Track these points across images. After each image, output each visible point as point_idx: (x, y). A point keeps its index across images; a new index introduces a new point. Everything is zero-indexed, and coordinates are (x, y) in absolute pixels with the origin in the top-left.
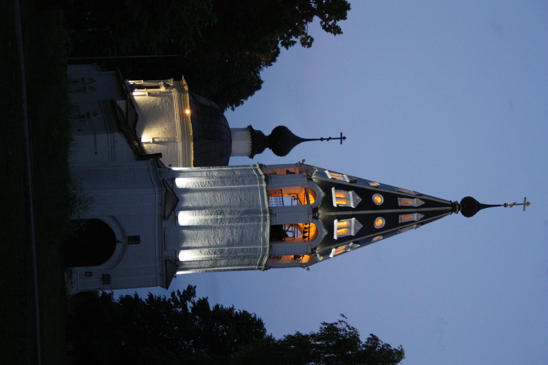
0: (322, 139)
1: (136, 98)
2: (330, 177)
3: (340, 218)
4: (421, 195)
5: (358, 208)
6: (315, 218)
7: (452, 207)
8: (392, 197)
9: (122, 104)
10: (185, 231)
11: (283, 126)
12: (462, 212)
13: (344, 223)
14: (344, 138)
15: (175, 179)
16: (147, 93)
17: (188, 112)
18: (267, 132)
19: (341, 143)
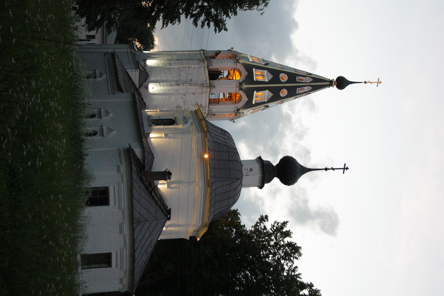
0: (326, 169)
1: (152, 140)
2: (251, 60)
3: (259, 90)
4: (311, 74)
5: (270, 82)
7: (330, 83)
8: (293, 76)
9: (138, 151)
10: (152, 96)
11: (343, 89)
12: (337, 86)
15: (146, 60)
17: (206, 156)
18: (275, 162)
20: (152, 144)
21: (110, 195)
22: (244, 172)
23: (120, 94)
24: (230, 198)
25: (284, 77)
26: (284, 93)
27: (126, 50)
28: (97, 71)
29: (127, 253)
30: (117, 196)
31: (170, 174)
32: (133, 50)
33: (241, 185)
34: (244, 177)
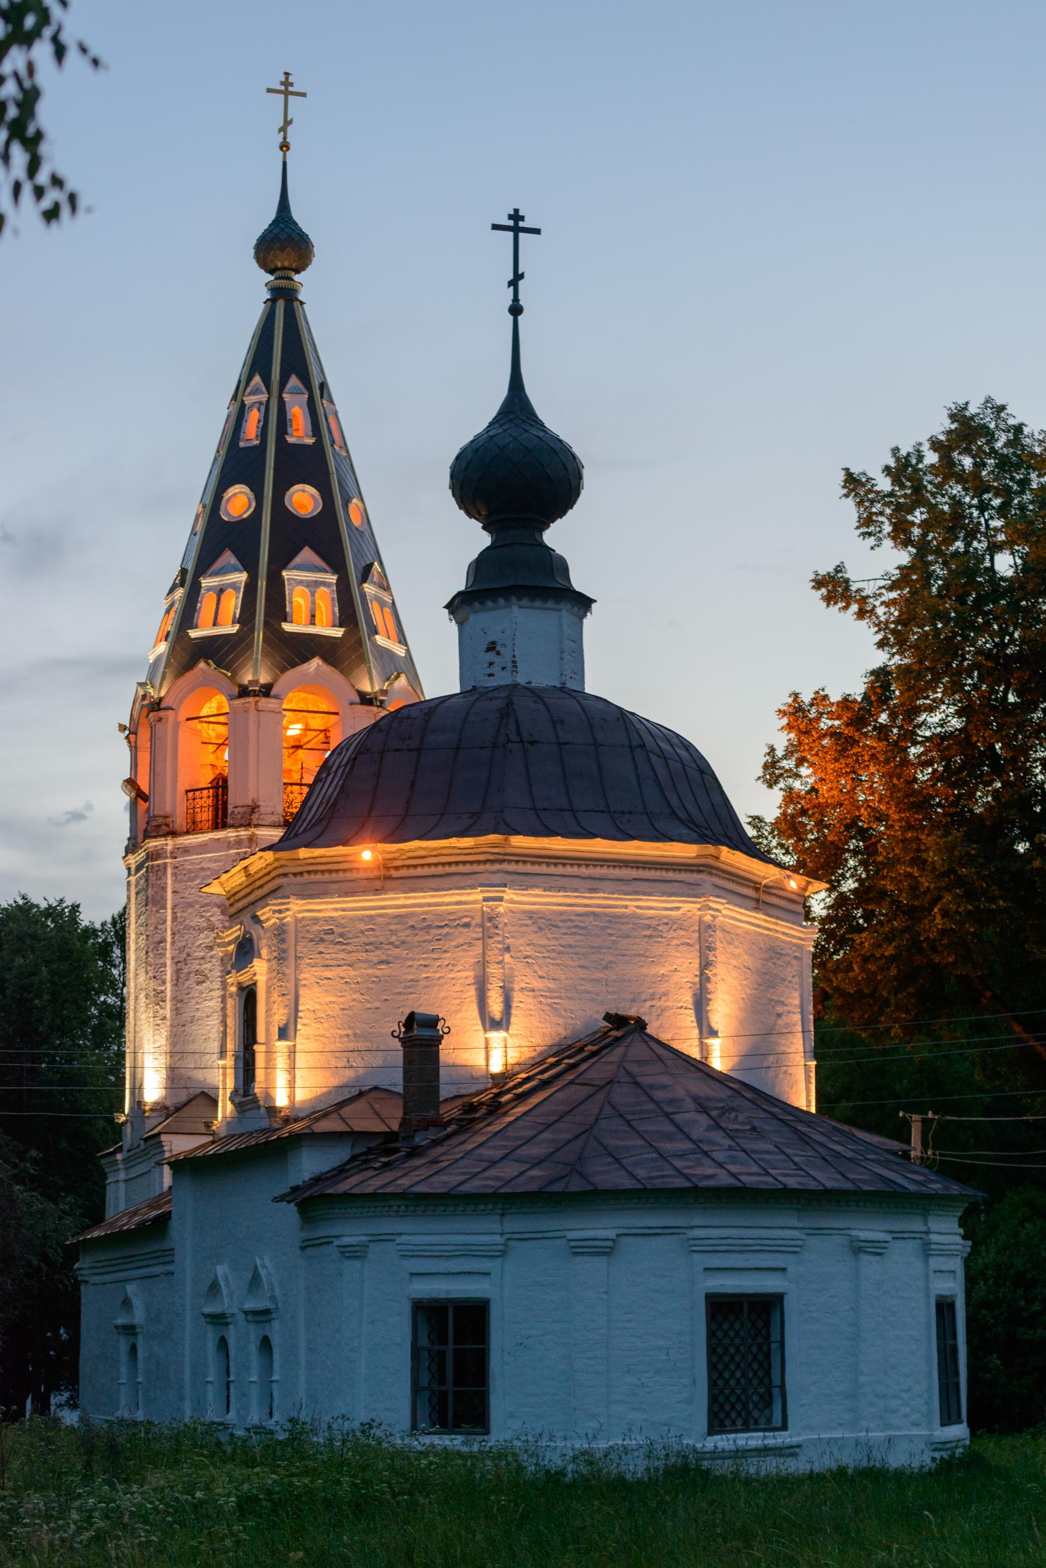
1: (301, 1095)
3: (278, 608)
5: (249, 564)
6: (266, 691)
7: (284, 298)
9: (309, 1164)
12: (297, 271)
13: (298, 599)
14: (516, 216)
16: (282, 1046)
18: (475, 538)
19: (537, 231)
20: (318, 1099)
21: (443, 1296)
22: (503, 679)
23: (174, 1224)
24: (596, 745)
25: (239, 501)
26: (303, 499)
27: (122, 1185)
28: (120, 1321)
29: (711, 1226)
30: (451, 1265)
31: (411, 1020)
32: (119, 1157)
33: (579, 696)
34: (521, 680)
